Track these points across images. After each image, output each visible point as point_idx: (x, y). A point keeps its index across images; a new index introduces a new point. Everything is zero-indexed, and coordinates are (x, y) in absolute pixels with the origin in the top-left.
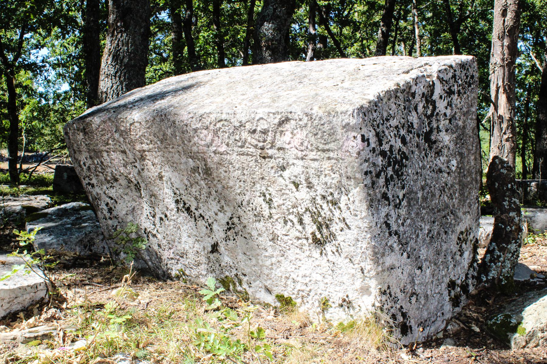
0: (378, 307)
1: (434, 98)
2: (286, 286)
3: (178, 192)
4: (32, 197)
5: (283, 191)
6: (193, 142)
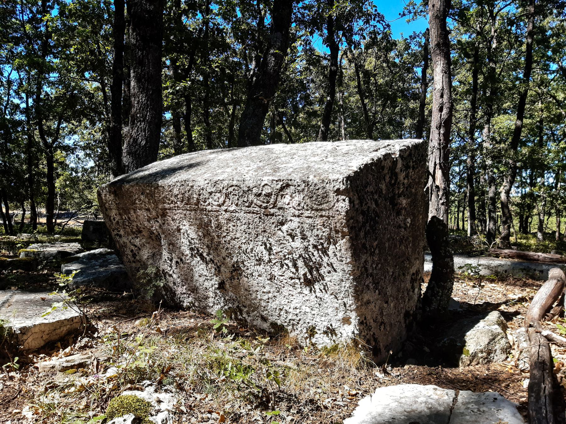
0: (357, 334)
1: (397, 170)
2: (280, 315)
3: (193, 241)
4: (66, 244)
5: (281, 241)
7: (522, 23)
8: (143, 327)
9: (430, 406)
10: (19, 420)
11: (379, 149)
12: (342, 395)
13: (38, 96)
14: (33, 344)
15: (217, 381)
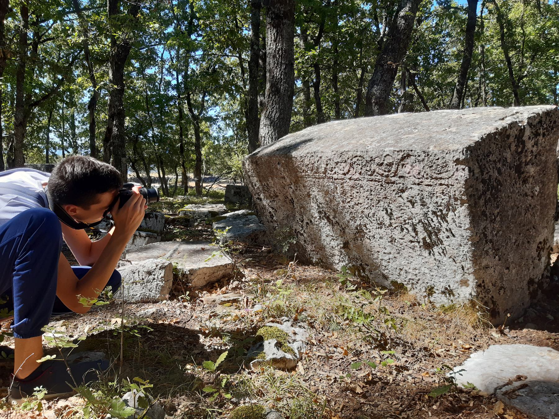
1: (524, 138)
2: (400, 275)
4: (214, 205)
5: (401, 207)
12: (456, 347)
13: (186, 73)
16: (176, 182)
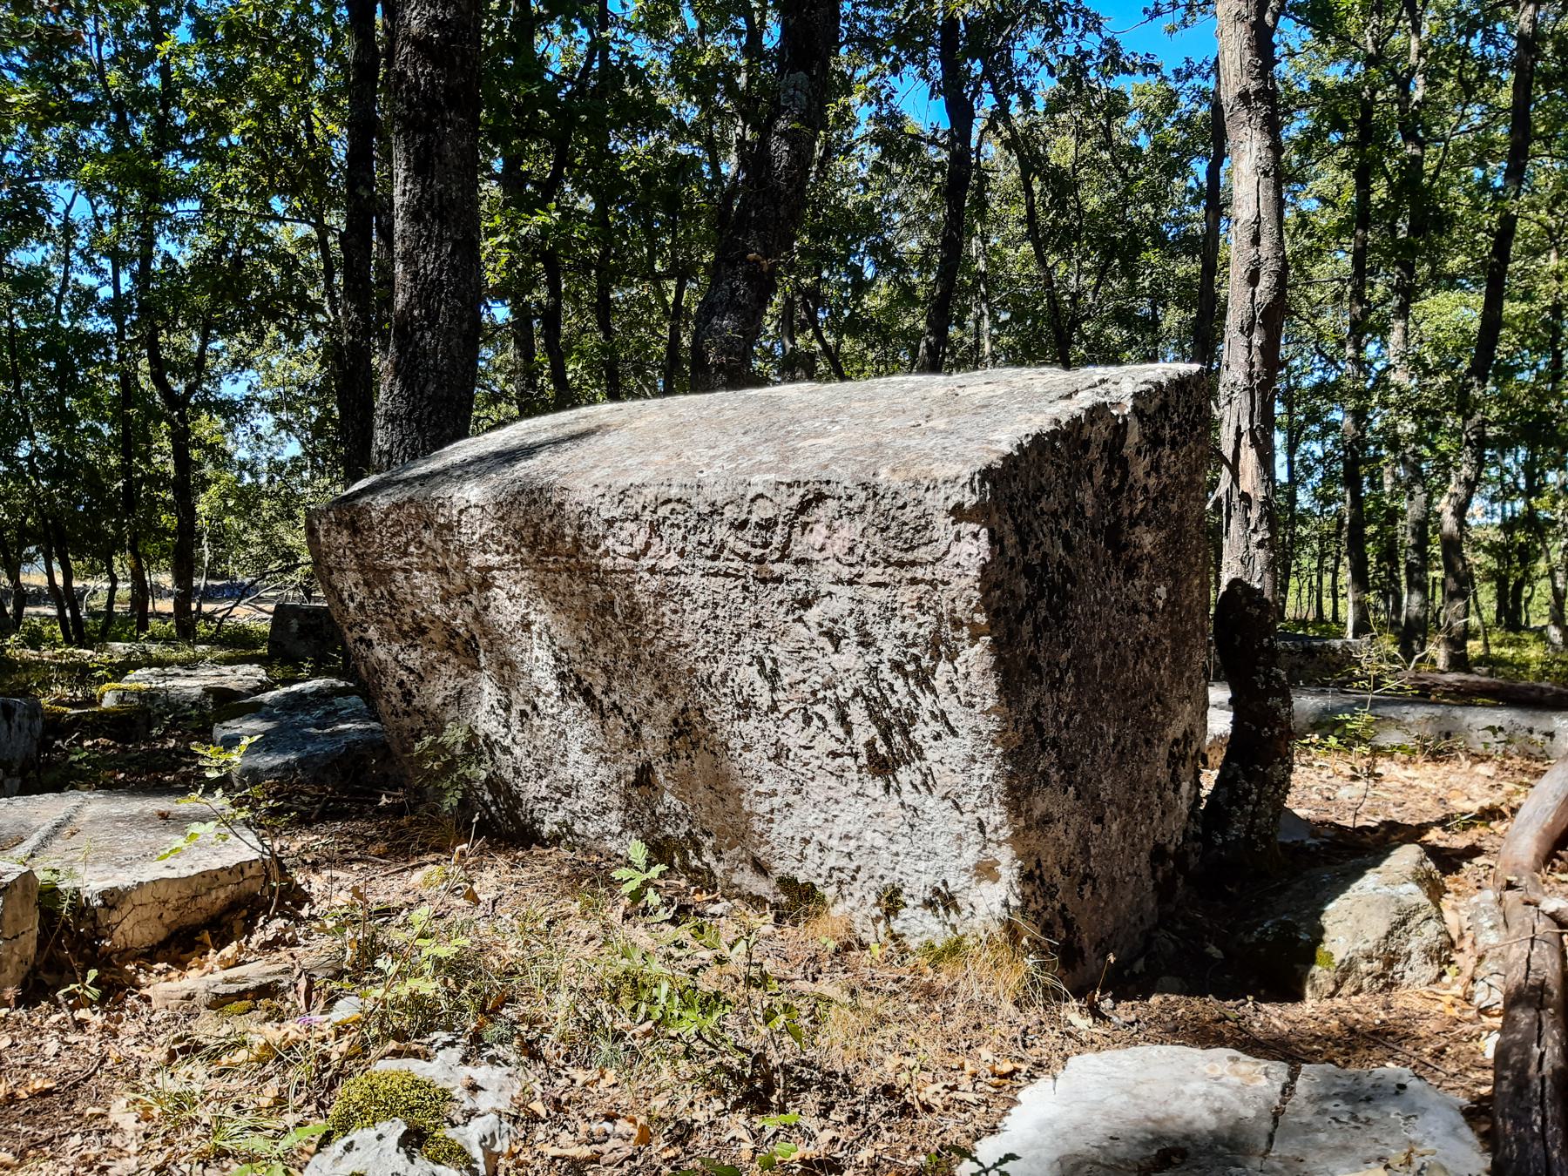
2: (802, 857)
4: (226, 669)
5: (804, 653)
6: (603, 548)
7: (1500, 27)
8: (433, 891)
9: (1217, 1105)
10: (102, 1133)
11: (1077, 392)
12: (974, 1075)
14: (138, 936)
15: (629, 1035)
16: (111, 602)
